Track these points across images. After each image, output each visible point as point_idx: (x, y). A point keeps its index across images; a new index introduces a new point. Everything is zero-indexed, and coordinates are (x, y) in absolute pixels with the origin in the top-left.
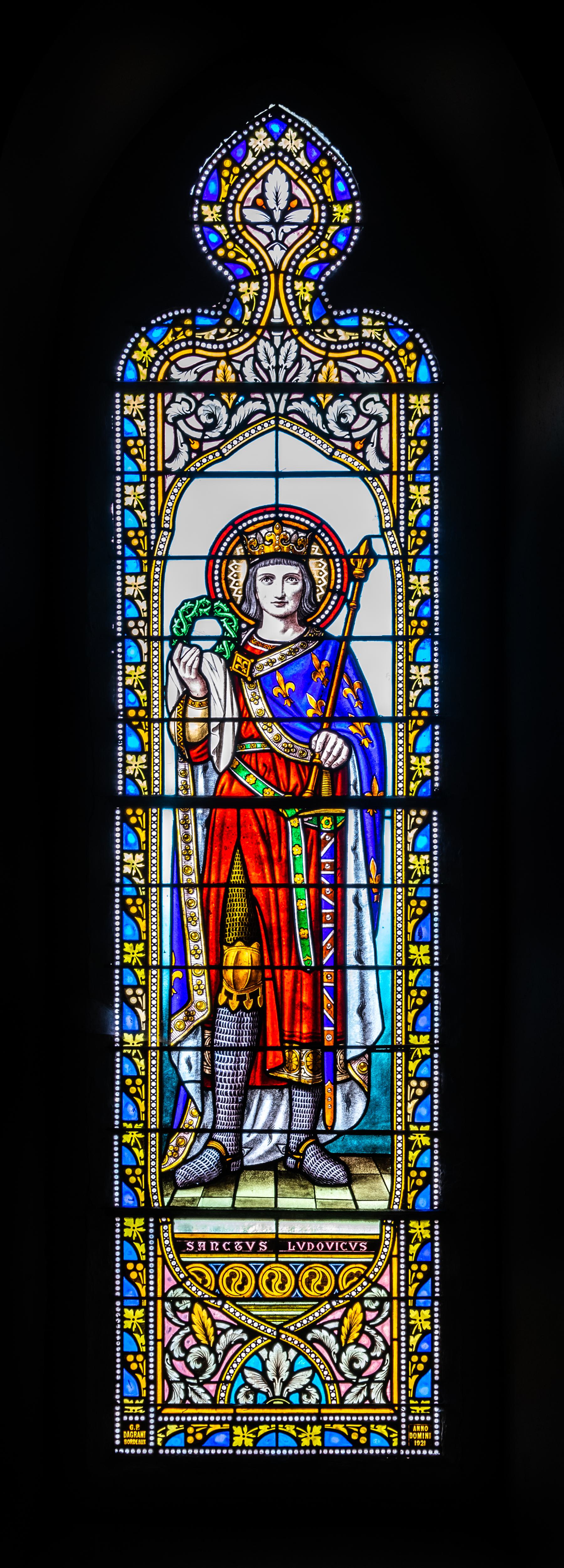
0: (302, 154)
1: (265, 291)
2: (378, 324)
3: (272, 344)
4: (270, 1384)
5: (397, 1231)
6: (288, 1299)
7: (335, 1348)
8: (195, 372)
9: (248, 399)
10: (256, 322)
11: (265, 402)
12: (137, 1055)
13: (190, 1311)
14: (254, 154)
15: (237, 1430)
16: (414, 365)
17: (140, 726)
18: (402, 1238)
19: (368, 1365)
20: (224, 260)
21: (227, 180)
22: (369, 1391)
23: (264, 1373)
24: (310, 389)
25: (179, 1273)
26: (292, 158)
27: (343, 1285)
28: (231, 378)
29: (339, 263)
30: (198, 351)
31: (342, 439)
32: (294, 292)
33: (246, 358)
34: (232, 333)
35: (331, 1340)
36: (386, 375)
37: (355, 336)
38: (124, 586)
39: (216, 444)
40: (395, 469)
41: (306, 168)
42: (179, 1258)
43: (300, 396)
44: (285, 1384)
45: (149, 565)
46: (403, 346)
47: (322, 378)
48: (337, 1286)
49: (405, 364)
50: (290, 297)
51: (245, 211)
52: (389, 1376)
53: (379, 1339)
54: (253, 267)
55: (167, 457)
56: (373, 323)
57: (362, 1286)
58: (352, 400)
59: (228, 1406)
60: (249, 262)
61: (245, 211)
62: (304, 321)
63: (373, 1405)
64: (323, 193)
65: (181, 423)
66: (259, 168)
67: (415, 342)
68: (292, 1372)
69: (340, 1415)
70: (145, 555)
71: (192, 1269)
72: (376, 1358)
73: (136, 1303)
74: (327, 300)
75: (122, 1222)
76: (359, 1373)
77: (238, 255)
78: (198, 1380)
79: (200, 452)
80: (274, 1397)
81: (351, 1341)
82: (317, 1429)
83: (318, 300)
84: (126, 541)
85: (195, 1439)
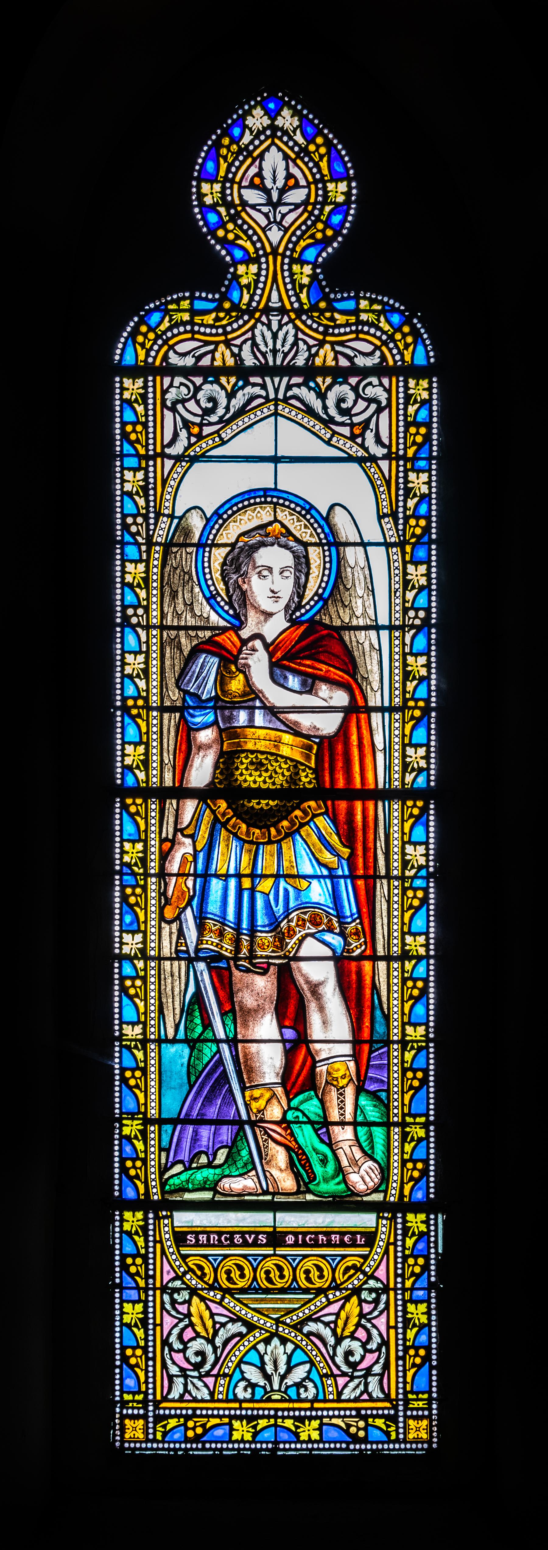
0: (298, 132)
1: (264, 273)
4: (268, 1377)
7: (331, 1341)
8: (193, 356)
9: (247, 383)
10: (254, 304)
11: (264, 386)
12: (136, 1047)
13: (189, 1302)
14: (251, 132)
16: (411, 348)
17: (139, 715)
19: (363, 1358)
20: (224, 242)
21: (225, 158)
22: (366, 1385)
24: (310, 372)
25: (180, 1267)
28: (230, 362)
29: (335, 245)
30: (196, 336)
32: (292, 275)
33: (245, 342)
34: (231, 317)
35: (327, 1333)
36: (383, 357)
37: (353, 319)
38: (124, 572)
42: (179, 1251)
44: (283, 1377)
45: (148, 552)
47: (318, 361)
48: (334, 1279)
49: (402, 348)
50: (288, 280)
51: (243, 191)
52: (386, 1366)
53: (374, 1332)
54: (251, 249)
55: (166, 441)
56: (371, 306)
57: (358, 1279)
58: (350, 384)
60: (248, 245)
61: (243, 191)
62: (301, 304)
64: (320, 171)
65: (179, 407)
66: (256, 148)
68: (289, 1369)
69: (339, 1409)
70: (144, 541)
71: (191, 1262)
72: (371, 1351)
75: (121, 1216)
76: (354, 1366)
77: (237, 237)
79: (200, 437)
80: (272, 1390)
81: (346, 1333)
84: (126, 527)
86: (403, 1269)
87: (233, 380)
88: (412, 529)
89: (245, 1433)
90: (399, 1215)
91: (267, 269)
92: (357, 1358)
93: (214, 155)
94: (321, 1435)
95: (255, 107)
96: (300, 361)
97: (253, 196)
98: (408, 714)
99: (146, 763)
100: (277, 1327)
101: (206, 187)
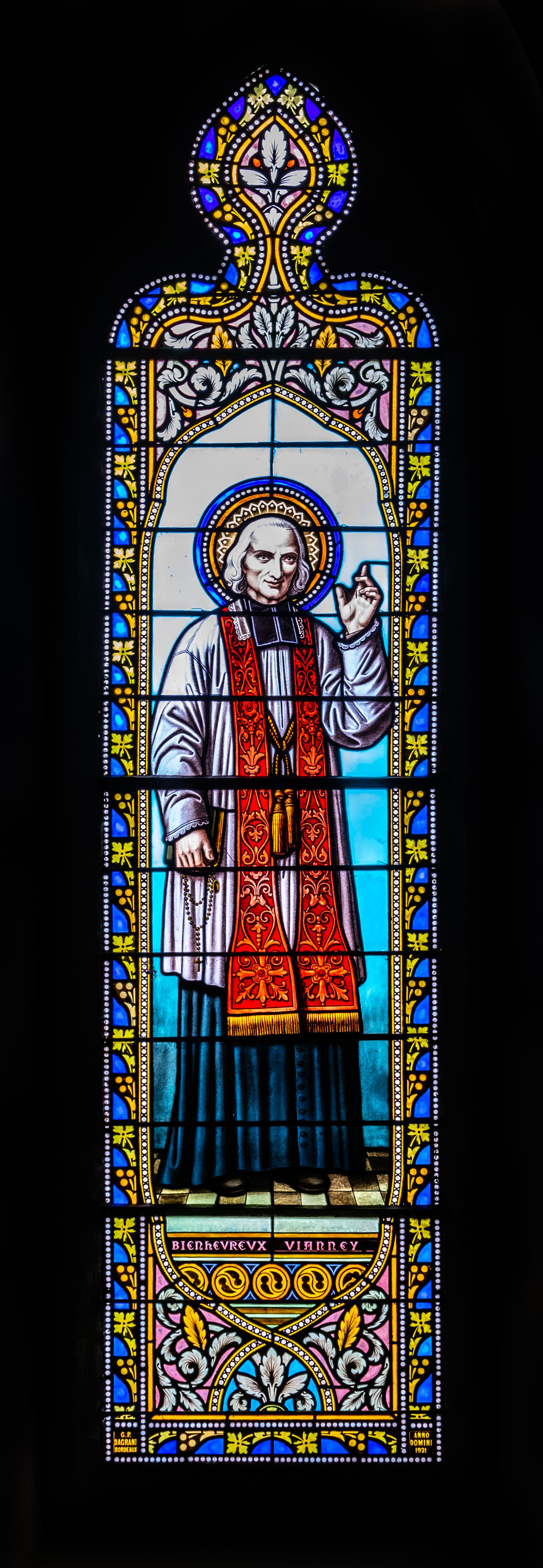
0: (301, 112)
1: (262, 255)
2: (376, 288)
3: (269, 310)
4: (264, 1389)
5: (396, 1232)
6: (283, 1301)
7: (332, 1352)
8: (191, 339)
9: (243, 366)
10: (252, 287)
11: (261, 369)
13: (182, 1312)
14: (253, 110)
15: (231, 1437)
18: (402, 1237)
19: (366, 1370)
20: (220, 223)
23: (258, 1379)
24: (308, 356)
25: (172, 1274)
26: (291, 116)
27: (340, 1286)
28: (228, 345)
30: (192, 318)
31: (341, 408)
32: (291, 257)
33: (242, 325)
35: (328, 1345)
36: (386, 339)
37: (354, 300)
39: (209, 412)
40: (394, 438)
41: (305, 126)
43: (299, 363)
44: (280, 1389)
45: (139, 537)
46: (403, 310)
47: (320, 344)
48: (334, 1287)
49: (405, 328)
50: (286, 262)
51: (242, 171)
52: (389, 1381)
54: (249, 231)
55: (159, 424)
56: (372, 287)
57: (361, 1286)
58: (350, 367)
59: (221, 1413)
60: (246, 226)
61: (242, 171)
62: (301, 286)
63: (372, 1412)
65: (173, 390)
67: (416, 306)
68: (287, 1379)
69: (338, 1421)
70: (135, 526)
72: (374, 1364)
73: (127, 1306)
74: (324, 264)
76: (357, 1378)
77: (236, 219)
78: (191, 1385)
79: (193, 421)
80: (269, 1402)
81: (348, 1345)
82: (313, 1436)
83: (315, 264)
85: (188, 1447)
86: (406, 1276)
87: (229, 363)
88: (413, 513)
89: (240, 1446)
90: (402, 1220)
91: (265, 252)
92: (359, 1370)
93: (212, 134)
94: (319, 1448)
95: (256, 84)
96: (301, 343)
97: (253, 178)
98: (408, 703)
99: (133, 753)
100: (273, 1336)
101: (203, 168)
